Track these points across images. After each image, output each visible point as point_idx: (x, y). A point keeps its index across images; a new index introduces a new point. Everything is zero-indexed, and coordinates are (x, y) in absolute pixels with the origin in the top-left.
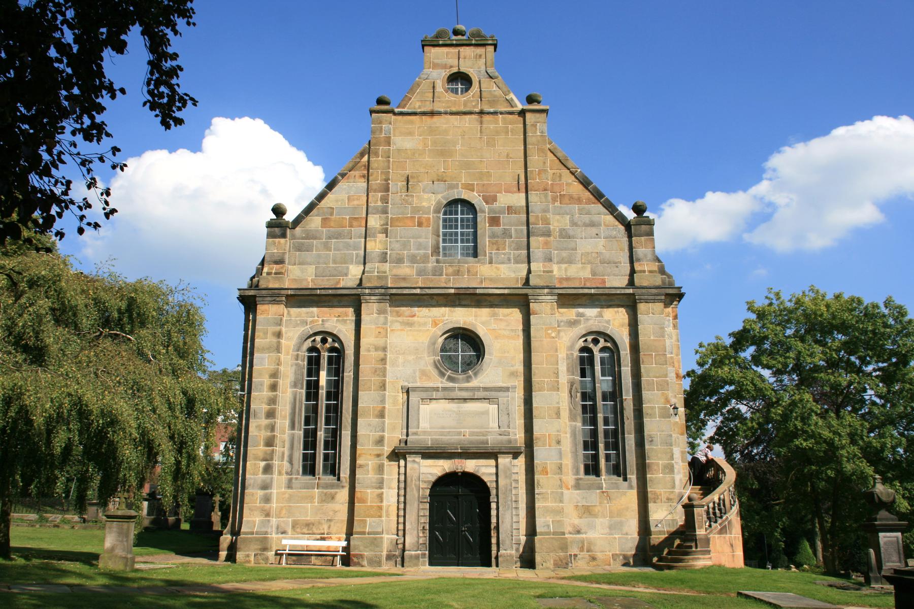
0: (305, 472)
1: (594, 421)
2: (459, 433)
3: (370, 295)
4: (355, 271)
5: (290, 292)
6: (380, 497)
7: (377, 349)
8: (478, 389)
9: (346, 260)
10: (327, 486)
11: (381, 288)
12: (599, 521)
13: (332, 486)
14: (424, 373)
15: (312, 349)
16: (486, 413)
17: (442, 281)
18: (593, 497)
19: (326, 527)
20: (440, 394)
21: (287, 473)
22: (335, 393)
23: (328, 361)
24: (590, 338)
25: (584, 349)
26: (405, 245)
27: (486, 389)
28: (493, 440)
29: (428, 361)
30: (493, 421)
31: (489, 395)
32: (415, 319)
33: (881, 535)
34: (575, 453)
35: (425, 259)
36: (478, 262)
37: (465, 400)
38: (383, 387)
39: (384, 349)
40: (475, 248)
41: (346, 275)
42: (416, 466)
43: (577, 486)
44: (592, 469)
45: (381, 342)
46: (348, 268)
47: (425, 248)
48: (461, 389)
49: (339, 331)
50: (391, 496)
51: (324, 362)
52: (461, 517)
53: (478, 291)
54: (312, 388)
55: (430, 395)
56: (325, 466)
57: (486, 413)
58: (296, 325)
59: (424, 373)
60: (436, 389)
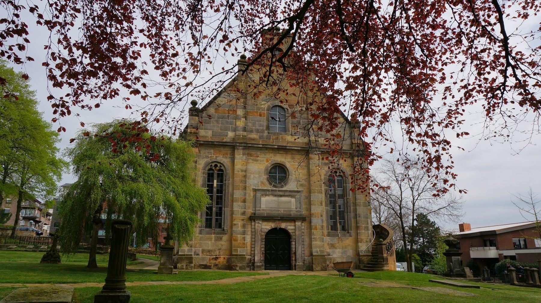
0: (206, 227)
1: (334, 207)
2: (279, 210)
3: (239, 146)
4: (231, 134)
5: (201, 142)
6: (244, 239)
7: (242, 171)
8: (287, 191)
9: (227, 129)
10: (218, 233)
11: (245, 143)
12: (337, 250)
13: (221, 234)
14: (262, 183)
15: (210, 169)
16: (290, 202)
17: (270, 142)
18: (335, 240)
19: (218, 252)
20: (270, 193)
21: (199, 227)
22: (220, 190)
23: (216, 174)
24: (213, 165)
25: (330, 175)
26: (254, 124)
27: (290, 191)
28: (293, 213)
29: (264, 177)
30: (290, 205)
31: (291, 194)
32: (259, 158)
33: (453, 257)
34: (327, 221)
35: (263, 132)
36: (286, 134)
37: (281, 196)
38: (245, 188)
39: (246, 171)
40: (285, 128)
41: (227, 136)
42: (260, 225)
43: (329, 235)
44: (334, 228)
45: (244, 168)
46: (227, 133)
47: (263, 126)
48: (279, 191)
49: (224, 162)
50: (248, 238)
51: (215, 176)
52: (279, 250)
53: (288, 148)
54: (210, 187)
55: (265, 193)
56: (216, 224)
57: (290, 202)
58: (203, 158)
59: (262, 183)
60: (268, 190)
